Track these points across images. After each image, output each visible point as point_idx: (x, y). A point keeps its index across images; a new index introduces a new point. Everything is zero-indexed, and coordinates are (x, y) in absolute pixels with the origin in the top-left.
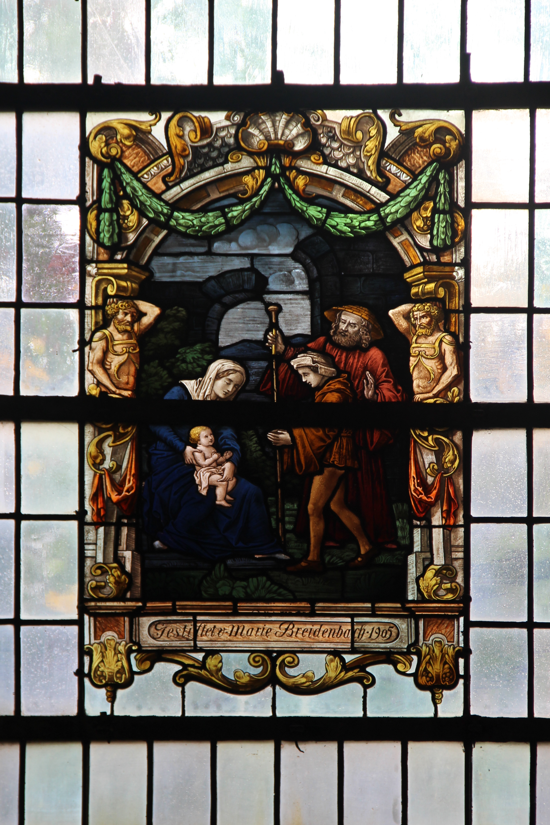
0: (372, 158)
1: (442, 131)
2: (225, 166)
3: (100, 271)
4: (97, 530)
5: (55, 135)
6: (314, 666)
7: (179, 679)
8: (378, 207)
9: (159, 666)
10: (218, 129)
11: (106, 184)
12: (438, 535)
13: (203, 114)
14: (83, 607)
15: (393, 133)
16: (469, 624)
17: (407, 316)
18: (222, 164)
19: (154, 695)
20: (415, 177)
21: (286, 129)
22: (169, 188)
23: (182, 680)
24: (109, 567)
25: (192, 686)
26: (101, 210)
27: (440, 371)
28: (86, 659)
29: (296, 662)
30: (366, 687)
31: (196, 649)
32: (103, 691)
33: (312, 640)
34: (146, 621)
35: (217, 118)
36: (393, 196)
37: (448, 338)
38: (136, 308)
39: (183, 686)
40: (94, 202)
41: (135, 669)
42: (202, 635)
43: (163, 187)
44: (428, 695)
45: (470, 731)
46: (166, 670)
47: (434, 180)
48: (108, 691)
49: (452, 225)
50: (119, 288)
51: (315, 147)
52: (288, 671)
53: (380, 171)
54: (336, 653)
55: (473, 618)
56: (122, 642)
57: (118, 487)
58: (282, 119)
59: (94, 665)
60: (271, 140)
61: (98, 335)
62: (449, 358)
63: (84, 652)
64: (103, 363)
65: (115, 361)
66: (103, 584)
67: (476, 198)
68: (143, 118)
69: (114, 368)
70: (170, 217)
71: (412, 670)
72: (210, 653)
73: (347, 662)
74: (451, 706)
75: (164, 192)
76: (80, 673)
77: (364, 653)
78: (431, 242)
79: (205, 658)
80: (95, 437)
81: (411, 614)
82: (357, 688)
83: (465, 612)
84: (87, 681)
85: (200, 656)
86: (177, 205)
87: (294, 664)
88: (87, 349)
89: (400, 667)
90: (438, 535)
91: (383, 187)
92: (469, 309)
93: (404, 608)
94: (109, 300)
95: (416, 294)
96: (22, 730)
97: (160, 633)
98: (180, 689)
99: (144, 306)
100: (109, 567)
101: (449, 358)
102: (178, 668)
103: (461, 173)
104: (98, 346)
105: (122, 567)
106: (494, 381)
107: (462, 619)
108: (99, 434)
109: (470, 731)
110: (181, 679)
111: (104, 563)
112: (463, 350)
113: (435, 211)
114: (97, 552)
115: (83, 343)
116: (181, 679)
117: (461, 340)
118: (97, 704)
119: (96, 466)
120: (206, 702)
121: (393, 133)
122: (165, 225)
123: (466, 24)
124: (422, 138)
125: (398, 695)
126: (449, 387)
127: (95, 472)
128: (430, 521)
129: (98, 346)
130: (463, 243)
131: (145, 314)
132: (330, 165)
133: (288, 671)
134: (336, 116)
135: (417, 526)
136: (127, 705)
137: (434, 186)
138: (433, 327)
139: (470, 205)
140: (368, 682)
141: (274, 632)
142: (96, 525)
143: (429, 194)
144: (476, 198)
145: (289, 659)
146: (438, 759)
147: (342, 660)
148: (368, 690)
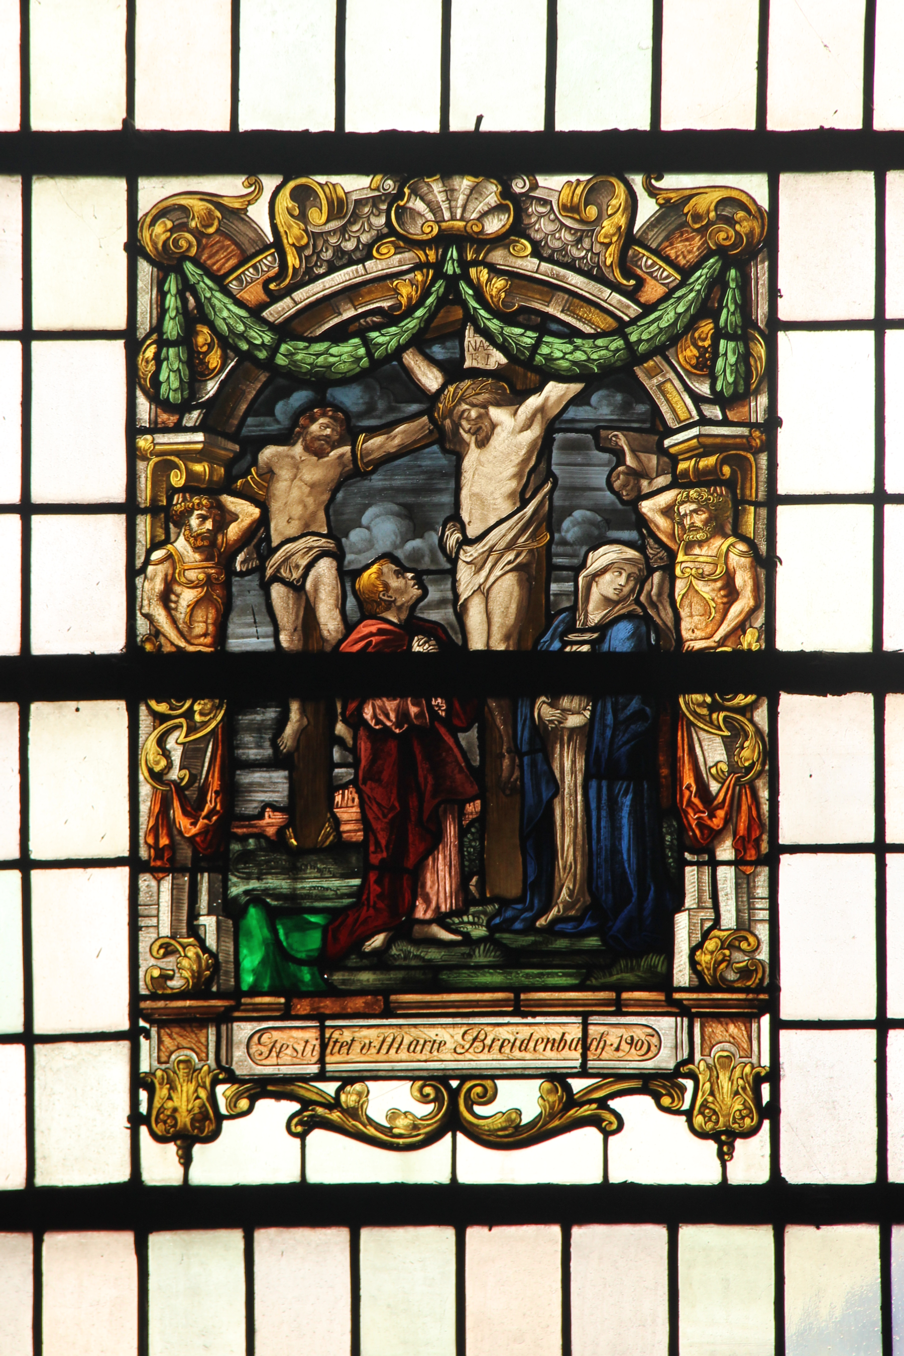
0: (612, 248)
1: (732, 203)
2: (367, 264)
3: (157, 447)
4: (159, 881)
5: (85, 220)
6: (523, 1099)
7: (296, 1125)
8: (621, 328)
9: (264, 1105)
10: (358, 202)
11: (171, 302)
12: (726, 875)
13: (334, 179)
14: (135, 1012)
15: (647, 208)
16: (778, 1025)
17: (668, 511)
18: (362, 261)
19: (255, 1149)
20: (686, 273)
21: (470, 201)
22: (274, 298)
23: (299, 1129)
24: (180, 944)
25: (317, 1136)
26: (163, 343)
27: (725, 600)
28: (143, 1095)
29: (490, 1093)
30: (607, 1134)
31: (322, 1076)
32: (172, 1148)
33: (521, 1052)
34: (243, 1030)
35: (354, 185)
36: (648, 309)
37: (742, 547)
38: (221, 507)
39: (302, 1136)
40: (152, 331)
41: (223, 1110)
42: (331, 1054)
43: (263, 297)
44: (711, 1146)
45: (781, 1205)
46: (274, 1112)
47: (717, 283)
48: (179, 1148)
49: (745, 357)
50: (190, 474)
51: (518, 229)
52: (478, 1109)
53: (625, 265)
54: (557, 1078)
55: (786, 1014)
56: (203, 1066)
57: (192, 810)
58: (464, 184)
59: (157, 1104)
60: (444, 221)
61: (157, 555)
62: (743, 580)
63: (138, 1081)
64: (166, 598)
65: (187, 596)
66: (171, 973)
67: (784, 315)
68: (229, 186)
69: (182, 611)
70: (274, 350)
71: (686, 1106)
72: (348, 1080)
73: (575, 1092)
74: (749, 1165)
75: (265, 306)
76: (136, 1120)
77: (604, 1076)
78: (713, 387)
79: (339, 1091)
80: (155, 729)
81: (682, 1010)
82: (591, 1134)
83: (772, 1006)
84: (144, 1130)
85: (330, 1088)
86: (285, 331)
87: (489, 1097)
88: (139, 581)
89: (666, 1101)
90: (726, 875)
91: (632, 294)
92: (774, 499)
93: (670, 1002)
94: (176, 497)
95: (686, 472)
96: (38, 1211)
97: (266, 1051)
98: (297, 1142)
99: (232, 503)
100: (180, 944)
101: (743, 580)
102: (295, 1106)
103: (761, 271)
104: (157, 574)
105: (201, 942)
106: (817, 614)
107: (765, 1020)
108: (161, 724)
109: (781, 1205)
110: (303, 1126)
111: (173, 937)
112: (766, 563)
113: (719, 334)
114: (163, 920)
115: (133, 572)
116: (303, 1126)
117: (763, 548)
118: (161, 1166)
119: (157, 777)
120: (339, 1161)
121: (647, 208)
122: (269, 364)
123: (758, 63)
124: (697, 217)
125: (656, 1147)
126: (741, 628)
127: (154, 787)
128: (712, 855)
129: (157, 574)
130: (765, 387)
131: (235, 517)
132: (542, 259)
133: (478, 1109)
134: (554, 184)
135: (691, 864)
136: (220, 1164)
137: (716, 294)
138: (716, 528)
139: (776, 325)
140: (609, 1126)
141: (448, 1042)
142: (157, 872)
143: (707, 309)
144: (784, 315)
145: (479, 1090)
146: (728, 1255)
147: (568, 1088)
148: (611, 1139)
